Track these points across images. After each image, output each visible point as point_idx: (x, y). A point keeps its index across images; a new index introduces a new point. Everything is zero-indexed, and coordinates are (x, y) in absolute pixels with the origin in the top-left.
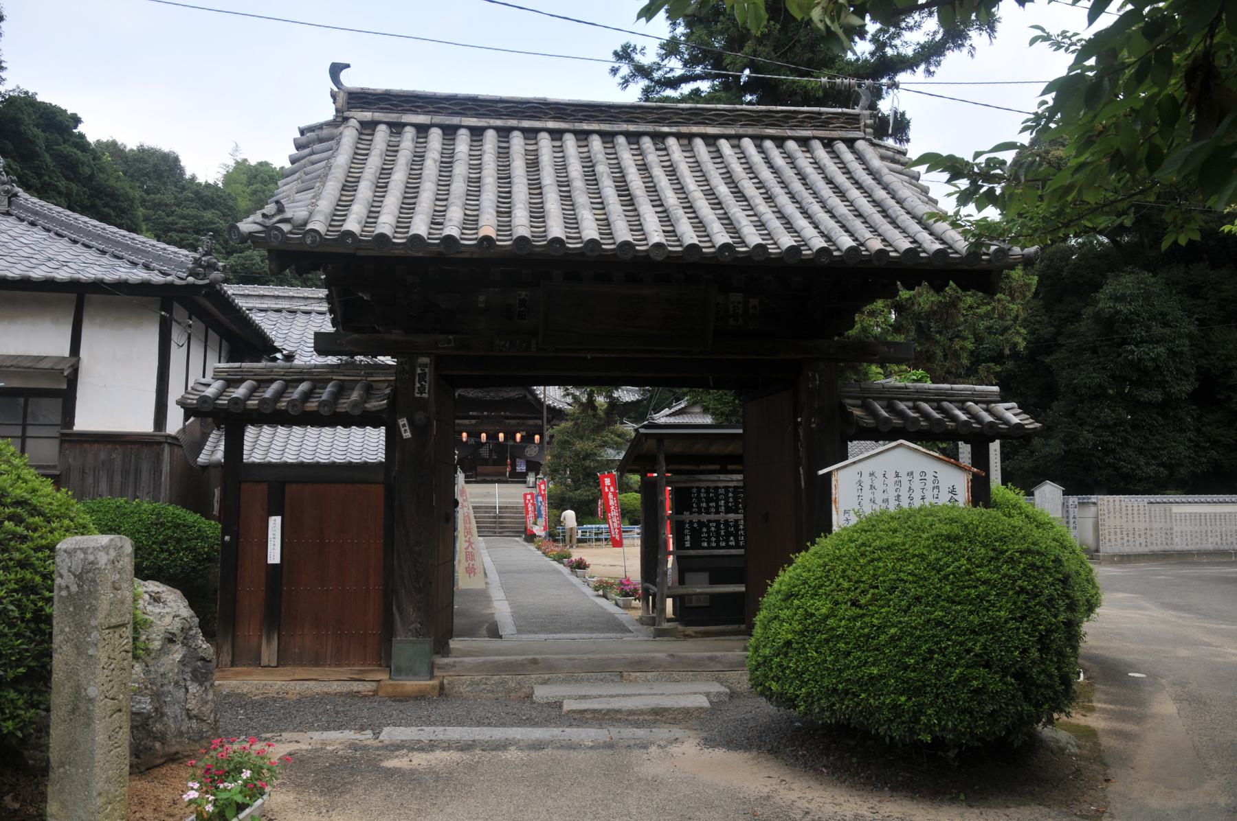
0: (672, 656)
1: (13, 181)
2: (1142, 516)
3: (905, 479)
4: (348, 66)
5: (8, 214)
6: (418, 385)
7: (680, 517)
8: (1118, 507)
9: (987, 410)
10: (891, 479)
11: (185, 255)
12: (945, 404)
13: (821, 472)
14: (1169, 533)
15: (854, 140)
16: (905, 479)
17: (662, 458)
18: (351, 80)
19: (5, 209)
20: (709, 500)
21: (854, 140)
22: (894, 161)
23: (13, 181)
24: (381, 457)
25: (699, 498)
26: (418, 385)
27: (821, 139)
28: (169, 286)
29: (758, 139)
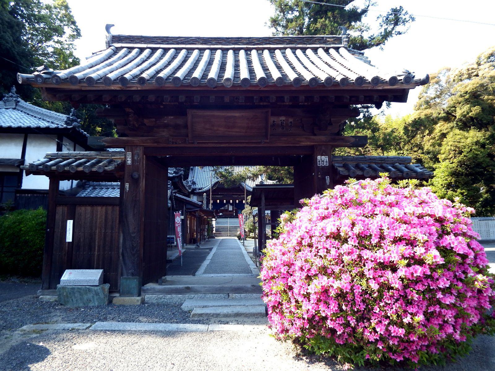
0: (253, 286)
1: (18, 97)
2: (476, 225)
4: (113, 25)
5: (14, 109)
9: (406, 167)
11: (64, 117)
12: (384, 165)
14: (488, 232)
15: (338, 48)
18: (115, 32)
19: (14, 107)
21: (338, 48)
23: (18, 97)
24: (61, 182)
27: (323, 48)
28: (57, 129)
29: (294, 50)
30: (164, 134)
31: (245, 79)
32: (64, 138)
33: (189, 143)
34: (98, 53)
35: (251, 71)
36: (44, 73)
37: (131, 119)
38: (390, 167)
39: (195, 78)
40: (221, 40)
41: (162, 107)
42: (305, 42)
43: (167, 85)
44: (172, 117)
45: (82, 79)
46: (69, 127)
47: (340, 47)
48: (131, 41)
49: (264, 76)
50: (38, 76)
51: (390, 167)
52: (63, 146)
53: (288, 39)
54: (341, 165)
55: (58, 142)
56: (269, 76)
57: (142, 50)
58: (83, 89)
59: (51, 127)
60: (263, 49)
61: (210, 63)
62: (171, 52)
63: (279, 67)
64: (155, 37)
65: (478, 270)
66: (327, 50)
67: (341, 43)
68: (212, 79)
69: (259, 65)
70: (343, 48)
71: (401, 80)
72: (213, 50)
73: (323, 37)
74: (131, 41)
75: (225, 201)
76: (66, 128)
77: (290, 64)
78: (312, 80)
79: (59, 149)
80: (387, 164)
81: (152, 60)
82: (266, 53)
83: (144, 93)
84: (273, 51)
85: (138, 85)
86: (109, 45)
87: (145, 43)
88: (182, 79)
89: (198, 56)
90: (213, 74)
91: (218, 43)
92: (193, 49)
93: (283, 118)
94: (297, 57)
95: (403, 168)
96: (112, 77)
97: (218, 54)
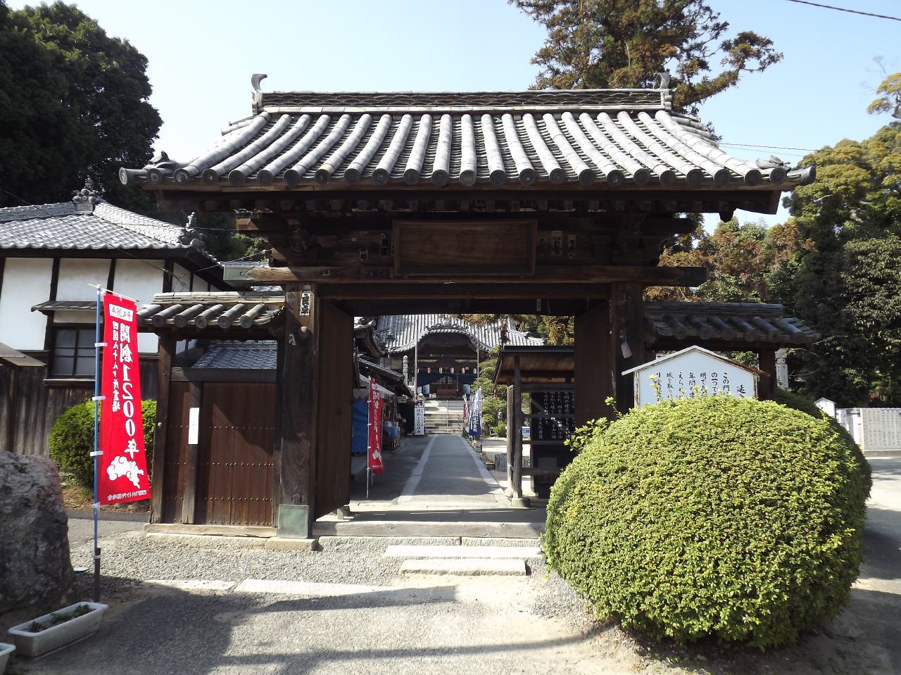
3: (698, 378)
4: (265, 76)
6: (302, 306)
7: (535, 416)
8: (876, 416)
9: (772, 323)
10: (686, 379)
12: (734, 318)
13: (624, 373)
16: (698, 378)
17: (517, 372)
18: (267, 87)
19: (90, 212)
20: (557, 404)
22: (689, 125)
25: (549, 401)
26: (302, 306)
27: (628, 111)
29: (576, 114)
30: (352, 261)
31: (497, 173)
32: (176, 265)
33: (396, 278)
34: (240, 124)
35: (505, 155)
36: (160, 167)
37: (296, 237)
38: (745, 324)
39: (411, 171)
40: (449, 98)
41: (349, 215)
42: (596, 101)
43: (367, 182)
44: (365, 232)
45: (223, 175)
46: (185, 247)
47: (657, 110)
48: (295, 101)
49: (529, 166)
50: (153, 170)
51: (745, 324)
52: (174, 280)
53: (566, 96)
54: (660, 317)
55: (165, 273)
56: (536, 164)
57: (314, 117)
58: (226, 190)
59: (155, 247)
60: (522, 113)
61: (432, 139)
62: (364, 118)
63: (552, 147)
64: (335, 95)
65: (675, 573)
66: (634, 115)
67: (659, 102)
68: (439, 172)
69: (518, 144)
70: (664, 112)
71: (767, 175)
72: (436, 116)
73: (628, 93)
74: (295, 101)
75: (441, 370)
76: (180, 249)
77: (571, 140)
78: (613, 174)
79: (167, 287)
80: (741, 317)
81: (332, 136)
82: (528, 120)
83: (322, 197)
84: (539, 116)
85: (316, 184)
86: (258, 110)
87: (319, 105)
88: (389, 172)
89: (410, 127)
90: (439, 164)
91: (444, 102)
92: (402, 114)
93: (558, 234)
94: (582, 128)
95: (768, 325)
96: (273, 170)
97: (444, 123)
